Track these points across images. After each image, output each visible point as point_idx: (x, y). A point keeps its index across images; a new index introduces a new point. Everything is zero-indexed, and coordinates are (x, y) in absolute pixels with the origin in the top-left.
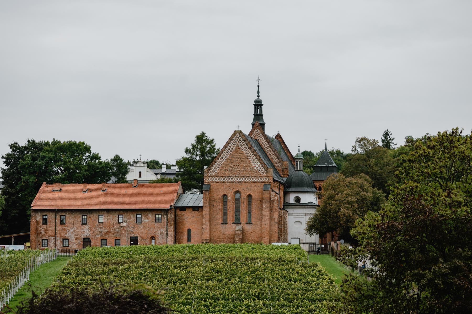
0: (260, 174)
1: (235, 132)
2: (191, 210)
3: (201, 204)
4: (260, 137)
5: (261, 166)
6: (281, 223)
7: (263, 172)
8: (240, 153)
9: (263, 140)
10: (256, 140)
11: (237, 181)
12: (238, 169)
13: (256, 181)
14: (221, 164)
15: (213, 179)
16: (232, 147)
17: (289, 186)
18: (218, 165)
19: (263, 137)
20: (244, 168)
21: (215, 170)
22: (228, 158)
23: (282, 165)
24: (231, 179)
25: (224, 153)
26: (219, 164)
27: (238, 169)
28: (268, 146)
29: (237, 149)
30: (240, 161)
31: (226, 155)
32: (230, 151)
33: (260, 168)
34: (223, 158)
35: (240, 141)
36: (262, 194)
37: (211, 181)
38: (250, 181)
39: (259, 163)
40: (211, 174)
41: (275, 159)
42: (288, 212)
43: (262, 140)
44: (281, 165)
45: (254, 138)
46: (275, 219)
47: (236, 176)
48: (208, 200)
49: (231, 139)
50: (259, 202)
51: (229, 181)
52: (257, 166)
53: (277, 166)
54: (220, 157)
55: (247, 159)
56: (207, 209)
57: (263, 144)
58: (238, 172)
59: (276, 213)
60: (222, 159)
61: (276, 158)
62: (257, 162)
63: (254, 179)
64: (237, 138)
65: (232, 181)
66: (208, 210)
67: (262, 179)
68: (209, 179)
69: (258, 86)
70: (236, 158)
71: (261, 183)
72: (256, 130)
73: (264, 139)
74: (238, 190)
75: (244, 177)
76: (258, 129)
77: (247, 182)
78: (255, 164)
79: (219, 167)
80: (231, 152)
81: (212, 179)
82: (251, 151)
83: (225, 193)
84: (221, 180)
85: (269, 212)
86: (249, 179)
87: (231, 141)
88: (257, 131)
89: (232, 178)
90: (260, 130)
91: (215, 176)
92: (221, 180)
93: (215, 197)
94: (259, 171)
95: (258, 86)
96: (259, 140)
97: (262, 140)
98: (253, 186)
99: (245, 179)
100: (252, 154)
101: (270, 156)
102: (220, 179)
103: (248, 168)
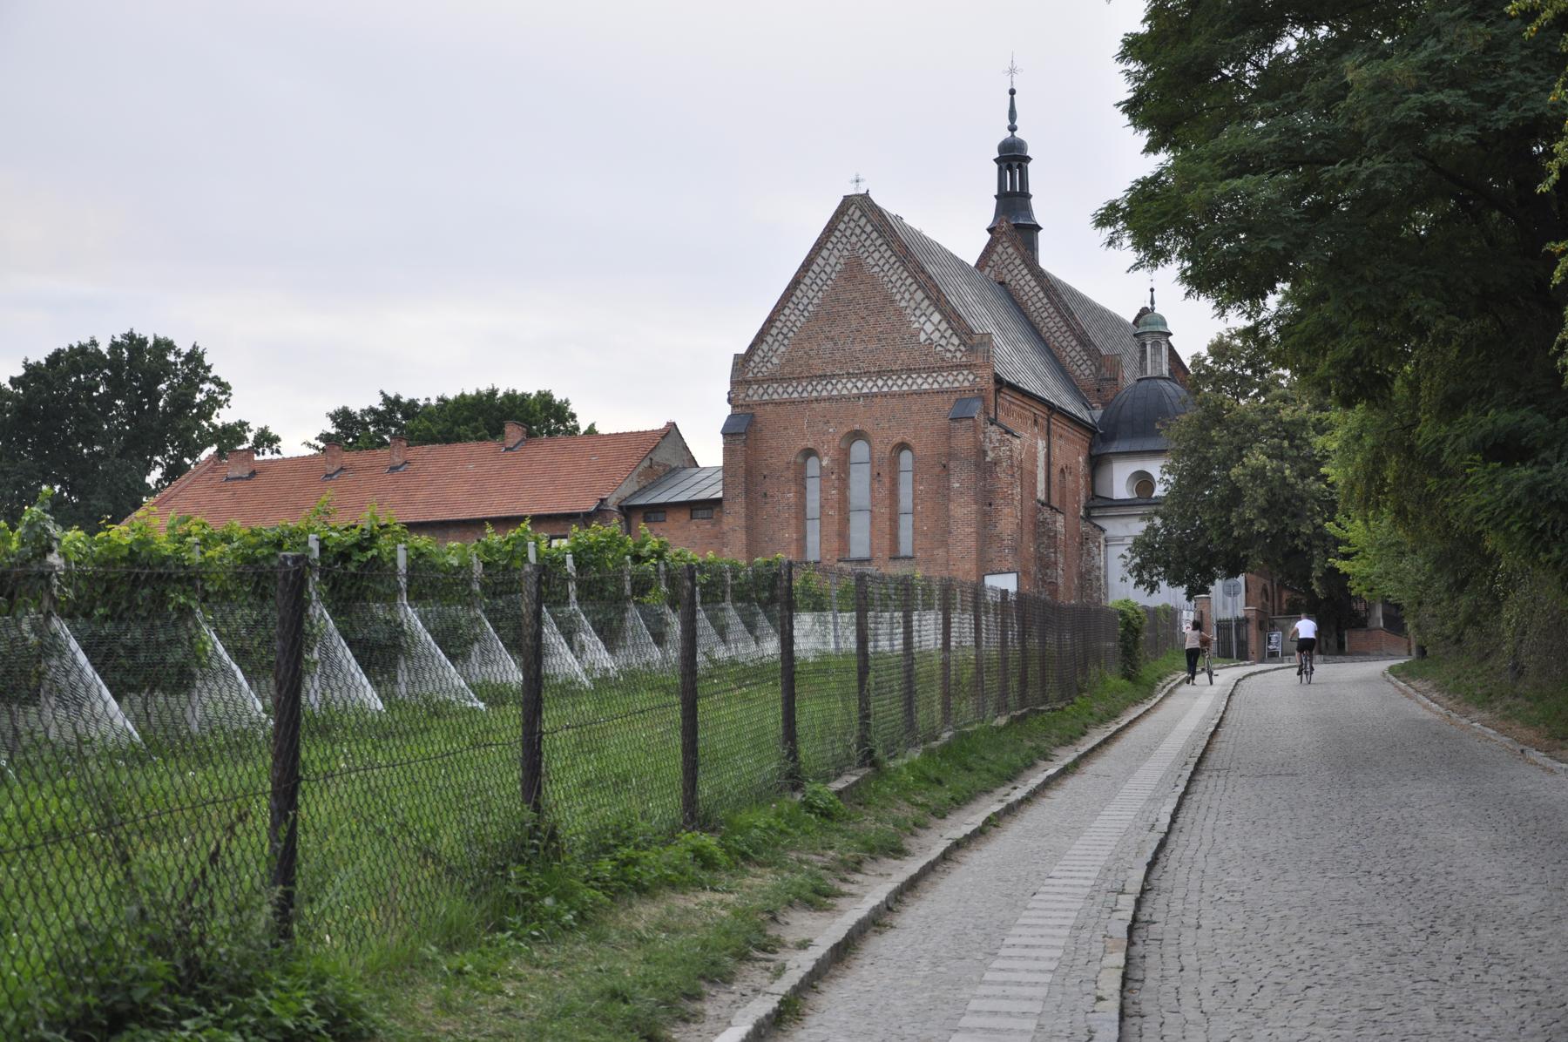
0: (943, 360)
1: (843, 201)
2: (683, 517)
3: (720, 495)
4: (1016, 272)
5: (944, 326)
6: (1056, 563)
7: (952, 349)
8: (862, 282)
9: (1027, 283)
10: (1002, 283)
11: (855, 391)
12: (858, 347)
13: (925, 386)
14: (795, 329)
15: (766, 391)
16: (832, 261)
17: (1108, 438)
18: (780, 337)
19: (1025, 272)
20: (879, 340)
21: (770, 354)
22: (818, 305)
23: (1098, 370)
24: (829, 387)
25: (802, 286)
26: (785, 330)
27: (858, 347)
28: (1045, 301)
29: (854, 269)
30: (864, 313)
31: (811, 294)
32: (824, 277)
33: (942, 336)
34: (801, 307)
35: (864, 236)
36: (949, 435)
37: (756, 398)
38: (905, 388)
39: (936, 317)
40: (756, 370)
41: (1069, 349)
42: (1103, 530)
43: (1022, 282)
44: (1093, 368)
45: (992, 276)
46: (1005, 537)
47: (848, 374)
48: (741, 472)
49: (830, 229)
50: (938, 469)
51: (825, 393)
52: (929, 327)
53: (1078, 372)
54: (791, 305)
55: (893, 301)
56: (737, 508)
57: (1025, 298)
58: (858, 359)
59: (1007, 510)
60: (797, 312)
61: (1074, 343)
62: (928, 313)
63: (920, 381)
64: (852, 224)
65: (835, 393)
66: (742, 511)
67: (951, 378)
68: (751, 392)
69: (1012, 92)
70: (850, 302)
71: (946, 396)
72: (1000, 249)
73: (1028, 277)
74: (857, 427)
75: (880, 374)
76: (1006, 245)
77: (893, 395)
78: (923, 319)
79: (786, 342)
80: (829, 282)
81: (761, 391)
82: (906, 269)
83: (810, 445)
84: (794, 392)
85: (974, 507)
86: (900, 382)
87: (829, 237)
88: (1007, 250)
89: (834, 381)
90: (1014, 245)
91: (772, 379)
92: (794, 392)
93: (773, 460)
94: (939, 348)
95: (1012, 92)
96: (1013, 283)
97: (1022, 282)
98: (915, 408)
99: (885, 384)
100: (910, 280)
101: (1052, 339)
102: (790, 389)
103: (894, 339)
